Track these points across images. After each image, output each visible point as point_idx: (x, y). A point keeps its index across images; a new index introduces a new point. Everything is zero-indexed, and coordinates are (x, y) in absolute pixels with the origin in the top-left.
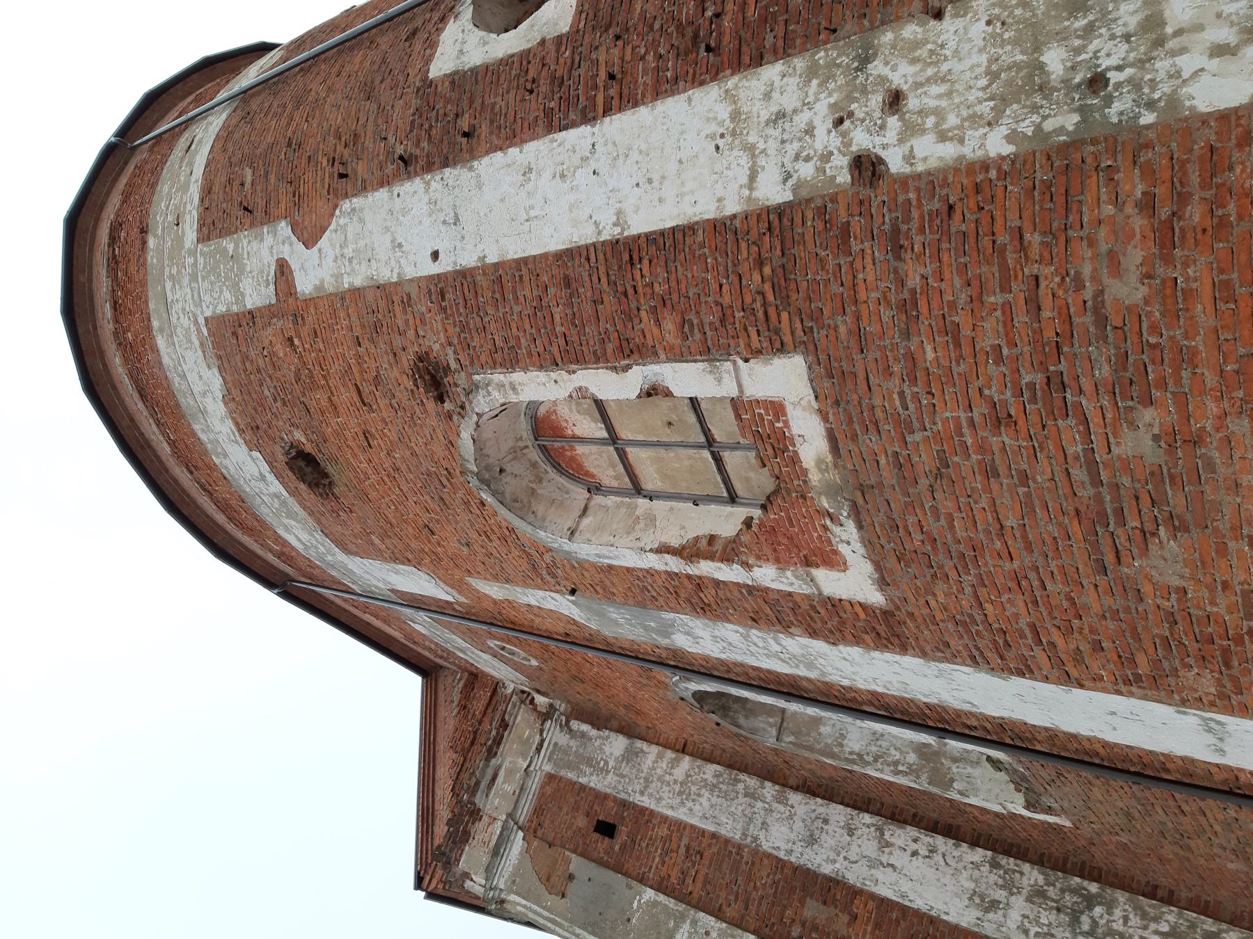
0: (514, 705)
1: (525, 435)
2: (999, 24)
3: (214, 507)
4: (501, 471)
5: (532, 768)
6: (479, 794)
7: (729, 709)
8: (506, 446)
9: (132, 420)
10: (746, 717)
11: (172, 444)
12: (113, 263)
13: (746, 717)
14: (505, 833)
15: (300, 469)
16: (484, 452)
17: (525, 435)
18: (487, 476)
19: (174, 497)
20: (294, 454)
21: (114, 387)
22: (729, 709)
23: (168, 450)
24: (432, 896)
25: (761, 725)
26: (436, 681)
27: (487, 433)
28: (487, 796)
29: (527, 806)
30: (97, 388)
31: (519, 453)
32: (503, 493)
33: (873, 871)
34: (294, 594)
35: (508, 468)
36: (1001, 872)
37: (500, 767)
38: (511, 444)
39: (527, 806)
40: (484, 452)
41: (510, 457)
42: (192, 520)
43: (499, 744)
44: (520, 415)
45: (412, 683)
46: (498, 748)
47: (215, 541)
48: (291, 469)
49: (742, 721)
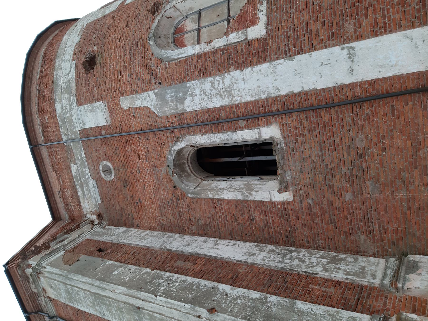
0: (86, 223)
1: (170, 34)
2: (382, 179)
3: (37, 102)
4: (159, 37)
5: (82, 235)
6: (53, 242)
7: (182, 177)
8: (164, 32)
9: (33, 69)
10: (187, 181)
11: (42, 74)
12: (45, 58)
13: (187, 181)
14: (57, 250)
15: (86, 66)
16: (159, 28)
17: (170, 34)
18: (155, 35)
19: (26, 97)
20: (87, 60)
21: (35, 59)
22: (182, 177)
23: (38, 77)
24: (8, 272)
25: (191, 185)
26: (56, 222)
27: (162, 23)
28: (56, 244)
29: (72, 246)
30: (30, 56)
31: (166, 37)
32: (157, 42)
33: (209, 250)
34: (35, 154)
35: (162, 38)
36: (259, 247)
37: (67, 238)
38: (166, 33)
39: (72, 246)
40: (159, 28)
41: (164, 36)
42: (25, 107)
43: (72, 231)
44: (172, 27)
45: (48, 219)
46: (71, 232)
47: (26, 118)
48: (83, 65)
49: (185, 182)
